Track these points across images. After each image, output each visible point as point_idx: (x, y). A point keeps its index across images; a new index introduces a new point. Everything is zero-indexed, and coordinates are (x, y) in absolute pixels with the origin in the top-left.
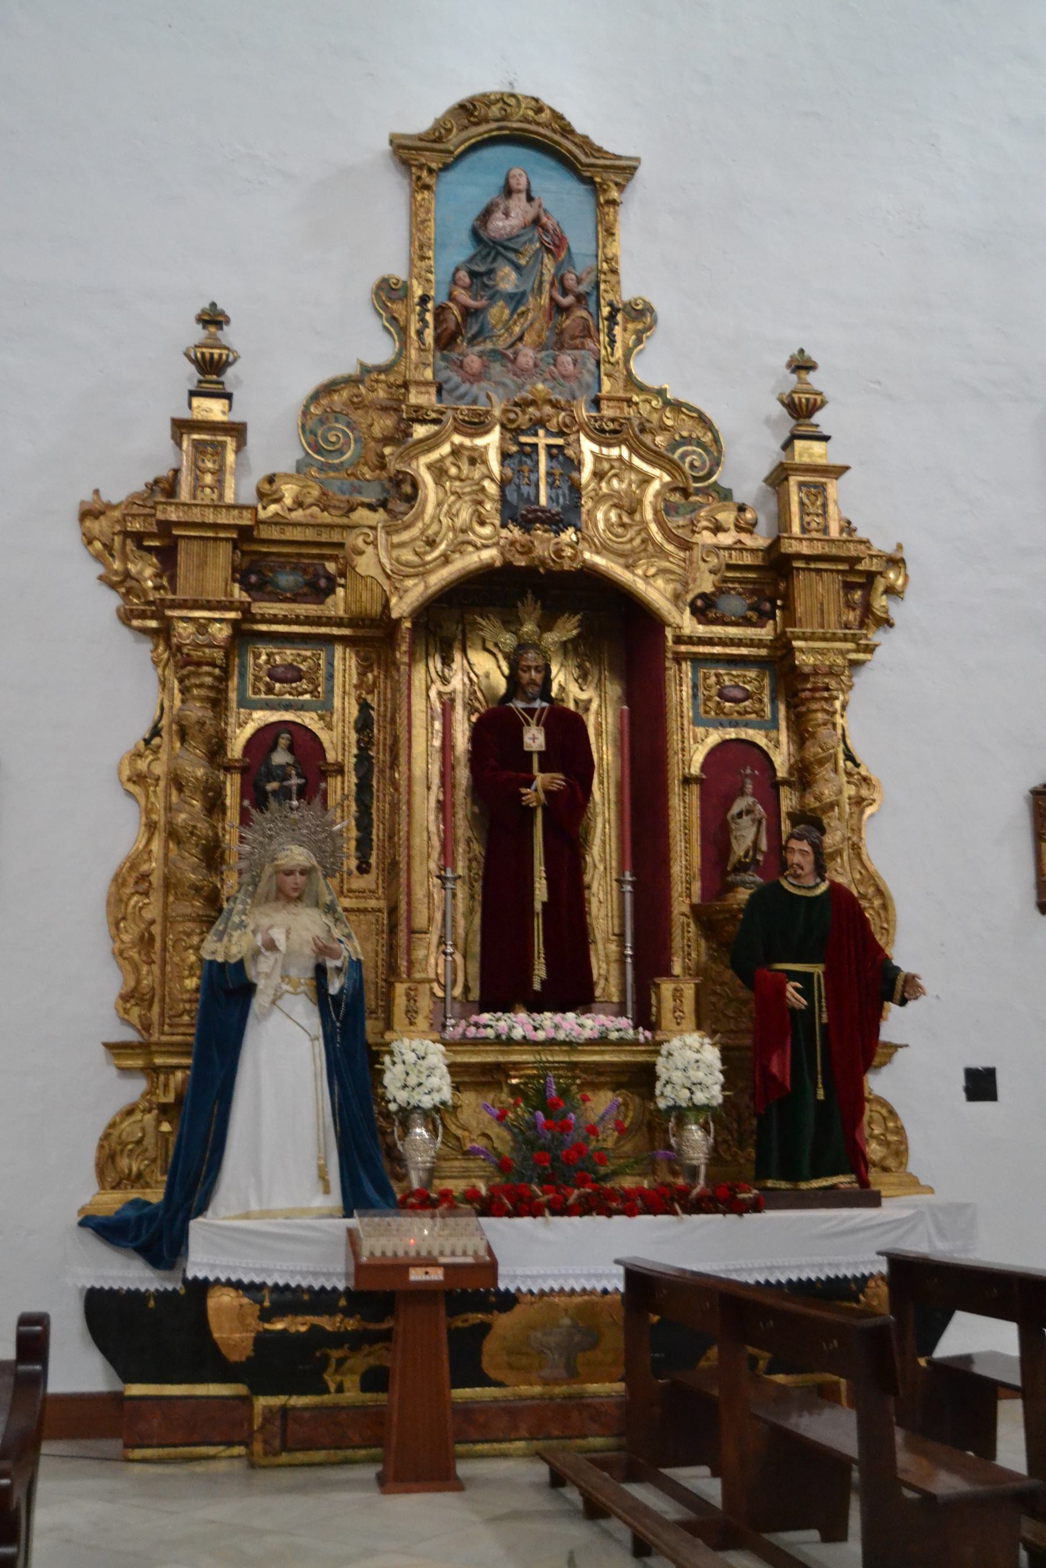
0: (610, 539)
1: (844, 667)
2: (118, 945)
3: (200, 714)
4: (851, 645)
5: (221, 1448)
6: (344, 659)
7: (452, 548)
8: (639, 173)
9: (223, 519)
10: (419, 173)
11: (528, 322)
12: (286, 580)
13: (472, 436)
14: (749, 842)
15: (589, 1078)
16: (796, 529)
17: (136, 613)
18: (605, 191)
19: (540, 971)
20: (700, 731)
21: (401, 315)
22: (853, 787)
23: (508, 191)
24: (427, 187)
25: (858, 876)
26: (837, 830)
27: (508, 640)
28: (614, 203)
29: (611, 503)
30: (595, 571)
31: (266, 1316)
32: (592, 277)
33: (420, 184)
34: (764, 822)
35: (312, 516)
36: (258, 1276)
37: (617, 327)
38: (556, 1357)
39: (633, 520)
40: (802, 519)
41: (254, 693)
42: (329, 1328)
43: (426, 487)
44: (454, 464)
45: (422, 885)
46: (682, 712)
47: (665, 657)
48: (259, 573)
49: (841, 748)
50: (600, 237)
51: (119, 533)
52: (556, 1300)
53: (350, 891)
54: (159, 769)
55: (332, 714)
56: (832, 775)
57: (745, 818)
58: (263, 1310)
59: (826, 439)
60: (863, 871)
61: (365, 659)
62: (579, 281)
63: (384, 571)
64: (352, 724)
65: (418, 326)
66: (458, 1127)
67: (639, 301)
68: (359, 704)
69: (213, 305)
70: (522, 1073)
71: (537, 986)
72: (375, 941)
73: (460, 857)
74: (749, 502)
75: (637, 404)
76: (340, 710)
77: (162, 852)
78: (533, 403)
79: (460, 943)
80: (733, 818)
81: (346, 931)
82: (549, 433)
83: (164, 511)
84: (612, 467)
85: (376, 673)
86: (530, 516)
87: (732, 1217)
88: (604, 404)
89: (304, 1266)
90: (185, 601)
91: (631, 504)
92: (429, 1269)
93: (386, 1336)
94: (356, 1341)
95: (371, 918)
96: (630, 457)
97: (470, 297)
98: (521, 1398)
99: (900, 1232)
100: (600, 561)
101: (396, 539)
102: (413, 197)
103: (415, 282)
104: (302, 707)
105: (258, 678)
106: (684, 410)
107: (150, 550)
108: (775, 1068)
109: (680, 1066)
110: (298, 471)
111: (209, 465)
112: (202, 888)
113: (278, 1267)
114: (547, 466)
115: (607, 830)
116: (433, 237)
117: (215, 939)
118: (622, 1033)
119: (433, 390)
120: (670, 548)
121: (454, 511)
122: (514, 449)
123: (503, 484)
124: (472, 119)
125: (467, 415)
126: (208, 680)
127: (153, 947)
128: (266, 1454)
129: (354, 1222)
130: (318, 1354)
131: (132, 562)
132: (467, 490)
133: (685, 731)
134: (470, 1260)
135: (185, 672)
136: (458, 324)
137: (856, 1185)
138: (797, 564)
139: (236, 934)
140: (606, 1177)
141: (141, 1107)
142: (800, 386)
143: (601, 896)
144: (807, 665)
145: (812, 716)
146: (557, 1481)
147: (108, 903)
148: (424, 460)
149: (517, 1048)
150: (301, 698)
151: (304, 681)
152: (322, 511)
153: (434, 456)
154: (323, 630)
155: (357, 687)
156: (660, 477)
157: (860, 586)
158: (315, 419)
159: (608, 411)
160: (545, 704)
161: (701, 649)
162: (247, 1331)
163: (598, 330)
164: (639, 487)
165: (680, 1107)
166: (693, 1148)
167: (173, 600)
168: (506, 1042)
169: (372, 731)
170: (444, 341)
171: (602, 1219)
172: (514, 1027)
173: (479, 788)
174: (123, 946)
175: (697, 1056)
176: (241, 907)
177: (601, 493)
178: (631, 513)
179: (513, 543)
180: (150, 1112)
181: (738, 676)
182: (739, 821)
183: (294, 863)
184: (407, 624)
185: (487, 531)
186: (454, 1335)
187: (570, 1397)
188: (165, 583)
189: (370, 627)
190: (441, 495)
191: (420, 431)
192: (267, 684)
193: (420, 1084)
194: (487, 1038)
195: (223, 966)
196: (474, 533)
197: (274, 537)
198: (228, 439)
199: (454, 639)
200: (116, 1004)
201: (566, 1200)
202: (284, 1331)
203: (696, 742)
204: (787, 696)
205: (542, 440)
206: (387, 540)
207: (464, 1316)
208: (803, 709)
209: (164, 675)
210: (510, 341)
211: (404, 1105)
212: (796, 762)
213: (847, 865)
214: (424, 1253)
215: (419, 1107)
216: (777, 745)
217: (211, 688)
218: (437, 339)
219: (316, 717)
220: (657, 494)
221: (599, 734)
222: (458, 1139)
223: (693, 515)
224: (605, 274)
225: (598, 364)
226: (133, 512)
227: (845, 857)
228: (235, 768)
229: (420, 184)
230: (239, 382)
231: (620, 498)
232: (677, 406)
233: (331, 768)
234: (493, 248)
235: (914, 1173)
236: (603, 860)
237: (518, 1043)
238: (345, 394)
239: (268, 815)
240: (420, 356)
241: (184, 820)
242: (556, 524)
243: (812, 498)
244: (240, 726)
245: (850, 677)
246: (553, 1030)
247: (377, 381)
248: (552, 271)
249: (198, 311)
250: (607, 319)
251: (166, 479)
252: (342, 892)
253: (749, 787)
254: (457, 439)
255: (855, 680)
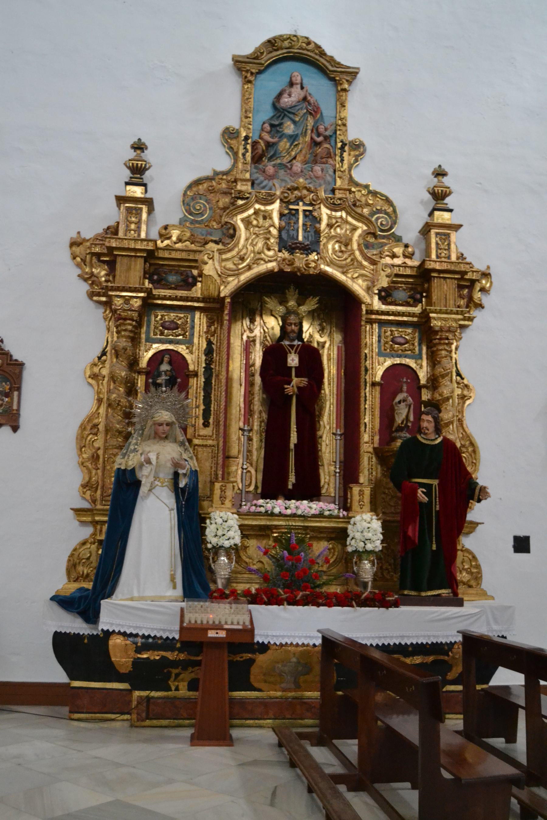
0: (334, 258)
1: (457, 328)
2: (81, 460)
3: (125, 344)
4: (460, 317)
5: (118, 715)
6: (200, 318)
7: (253, 262)
8: (359, 76)
9: (139, 246)
10: (246, 74)
11: (299, 150)
12: (172, 278)
13: (265, 205)
14: (404, 416)
15: (315, 535)
16: (434, 256)
17: (95, 293)
18: (341, 84)
19: (292, 479)
20: (382, 359)
21: (235, 146)
22: (460, 390)
23: (291, 84)
24: (250, 82)
25: (461, 436)
26: (450, 411)
27: (281, 309)
28: (345, 90)
29: (336, 240)
30: (325, 274)
31: (139, 650)
32: (333, 127)
33: (246, 80)
34: (412, 406)
35: (186, 246)
36: (134, 630)
37: (345, 153)
38: (289, 677)
39: (346, 248)
40: (437, 251)
41: (154, 335)
42: (171, 658)
43: (240, 231)
44: (255, 219)
45: (235, 434)
46: (372, 349)
47: (361, 320)
48: (158, 274)
49: (454, 370)
50: (338, 108)
51: (89, 253)
52: (290, 648)
53: (199, 436)
54: (105, 372)
55: (193, 346)
56: (449, 383)
57: (402, 403)
58: (137, 647)
59: (451, 211)
60: (464, 433)
61: (210, 319)
62: (326, 129)
63: (217, 272)
64: (203, 352)
65: (243, 151)
66: (247, 557)
67: (357, 140)
68: (207, 341)
69: (139, 140)
70: (279, 531)
71: (290, 487)
72: (210, 461)
73: (256, 420)
74: (410, 243)
75: (354, 192)
76: (197, 344)
77: (105, 413)
78: (297, 189)
79: (254, 464)
80: (396, 404)
81: (190, 455)
82: (305, 204)
83: (109, 242)
84: (337, 222)
85: (216, 326)
86: (293, 246)
87: (382, 610)
88: (337, 192)
89: (158, 626)
90: (118, 287)
91: (346, 240)
92: (218, 631)
93: (198, 664)
94: (185, 665)
95: (209, 450)
96: (346, 217)
97: (270, 137)
98: (271, 698)
99: (472, 620)
100: (329, 270)
101: (224, 257)
102: (243, 87)
103: (242, 129)
104: (178, 342)
105: (156, 328)
106: (378, 196)
107: (104, 262)
108: (410, 533)
109: (360, 530)
110: (180, 224)
111: (133, 219)
112: (122, 432)
113: (145, 626)
114: (303, 220)
115: (332, 409)
116: (252, 106)
117: (121, 457)
118: (331, 512)
119: (249, 184)
120: (365, 263)
121: (254, 243)
122: (286, 212)
123: (280, 230)
124: (274, 48)
125: (265, 196)
126: (130, 327)
127: (99, 461)
128: (138, 721)
129: (183, 604)
130: (165, 671)
131: (95, 268)
132: (261, 232)
133: (374, 359)
134: (240, 627)
135: (118, 323)
136: (263, 151)
137: (451, 594)
138: (434, 274)
139: (132, 455)
140: (320, 586)
141: (90, 541)
142: (438, 184)
143: (327, 442)
144: (437, 326)
145: (439, 353)
146: (280, 745)
147: (77, 438)
148: (240, 217)
149: (277, 518)
150: (177, 338)
151: (180, 329)
152: (191, 244)
153: (245, 215)
154: (189, 304)
155: (206, 333)
156: (362, 227)
157: (467, 287)
158: (190, 198)
159: (338, 194)
160: (300, 343)
161: (383, 317)
162: (129, 658)
163: (335, 155)
164: (350, 232)
165: (359, 551)
166: (365, 572)
167: (112, 287)
168: (270, 514)
169: (213, 355)
170: (256, 159)
171: (314, 608)
172: (275, 507)
173: (266, 386)
174: (83, 461)
175: (369, 525)
176: (135, 441)
177: (331, 235)
178: (346, 245)
179: (284, 260)
180: (94, 543)
181: (402, 332)
182: (399, 405)
183: (163, 419)
184: (228, 300)
185: (271, 253)
186: (231, 664)
187: (296, 698)
188: (111, 279)
189: (213, 302)
190: (248, 235)
191: (240, 202)
192: (161, 331)
193: (224, 535)
194: (260, 512)
195: (125, 470)
196: (265, 254)
197: (165, 256)
198: (144, 206)
199: (257, 309)
200: (79, 489)
201: (296, 597)
202: (148, 658)
203: (379, 365)
204: (427, 342)
205: (301, 207)
206: (219, 257)
207: (241, 655)
208: (435, 349)
209: (109, 325)
210: (290, 159)
211: (215, 545)
212: (430, 376)
213: (455, 430)
214: (217, 622)
215: (222, 547)
216: (421, 367)
217: (131, 331)
218: (253, 158)
219: (185, 348)
220: (360, 236)
221: (329, 360)
222: (246, 563)
223: (381, 249)
224: (339, 126)
225: (335, 171)
226: (95, 243)
227: (455, 426)
228: (143, 372)
229: (246, 80)
230: (152, 179)
231: (341, 238)
232: (375, 194)
233: (191, 373)
234: (283, 112)
235: (485, 589)
236: (329, 423)
237: (276, 515)
238: (205, 185)
239: (150, 395)
240: (244, 167)
241: (115, 398)
242: (307, 250)
243: (443, 241)
244: (146, 351)
245: (460, 333)
246: (295, 510)
247: (222, 179)
248: (312, 124)
249: (132, 143)
250: (340, 149)
251: (113, 227)
252: (195, 436)
253: (405, 388)
254: (257, 206)
255: (463, 335)
